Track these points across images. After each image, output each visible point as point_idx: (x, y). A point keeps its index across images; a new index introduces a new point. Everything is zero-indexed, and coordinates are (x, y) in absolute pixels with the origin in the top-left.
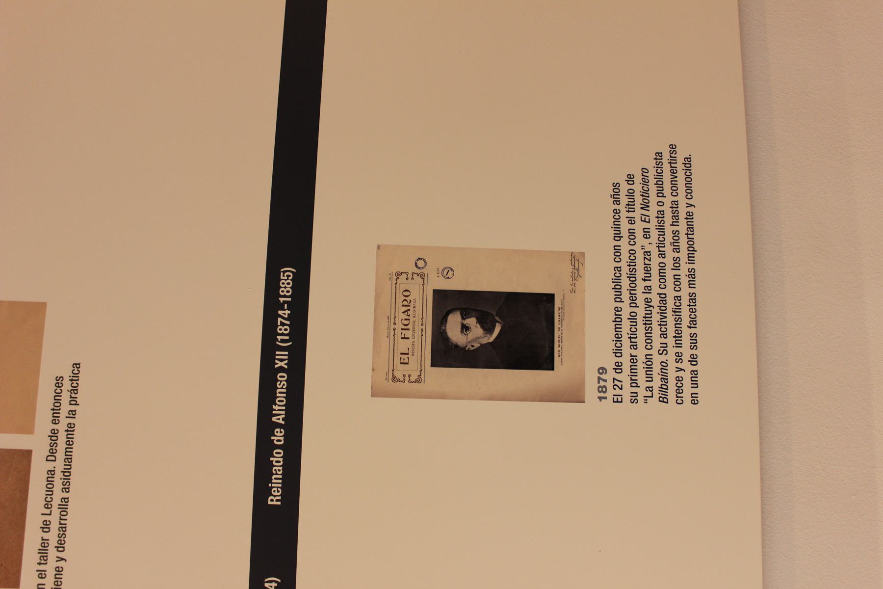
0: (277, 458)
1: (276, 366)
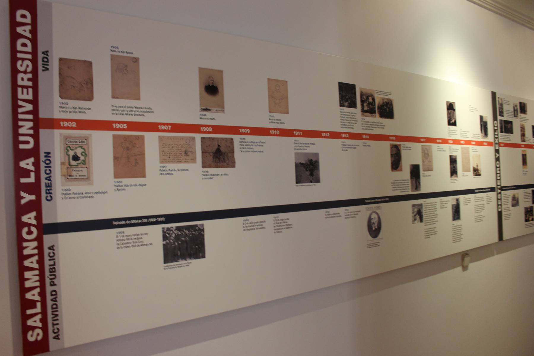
0: (123, 222)
1: (23, 202)
